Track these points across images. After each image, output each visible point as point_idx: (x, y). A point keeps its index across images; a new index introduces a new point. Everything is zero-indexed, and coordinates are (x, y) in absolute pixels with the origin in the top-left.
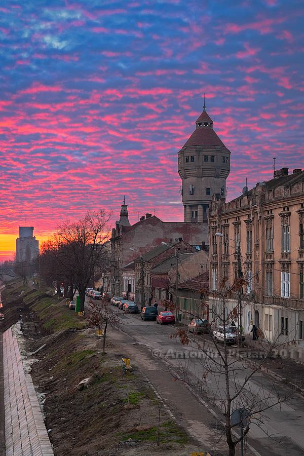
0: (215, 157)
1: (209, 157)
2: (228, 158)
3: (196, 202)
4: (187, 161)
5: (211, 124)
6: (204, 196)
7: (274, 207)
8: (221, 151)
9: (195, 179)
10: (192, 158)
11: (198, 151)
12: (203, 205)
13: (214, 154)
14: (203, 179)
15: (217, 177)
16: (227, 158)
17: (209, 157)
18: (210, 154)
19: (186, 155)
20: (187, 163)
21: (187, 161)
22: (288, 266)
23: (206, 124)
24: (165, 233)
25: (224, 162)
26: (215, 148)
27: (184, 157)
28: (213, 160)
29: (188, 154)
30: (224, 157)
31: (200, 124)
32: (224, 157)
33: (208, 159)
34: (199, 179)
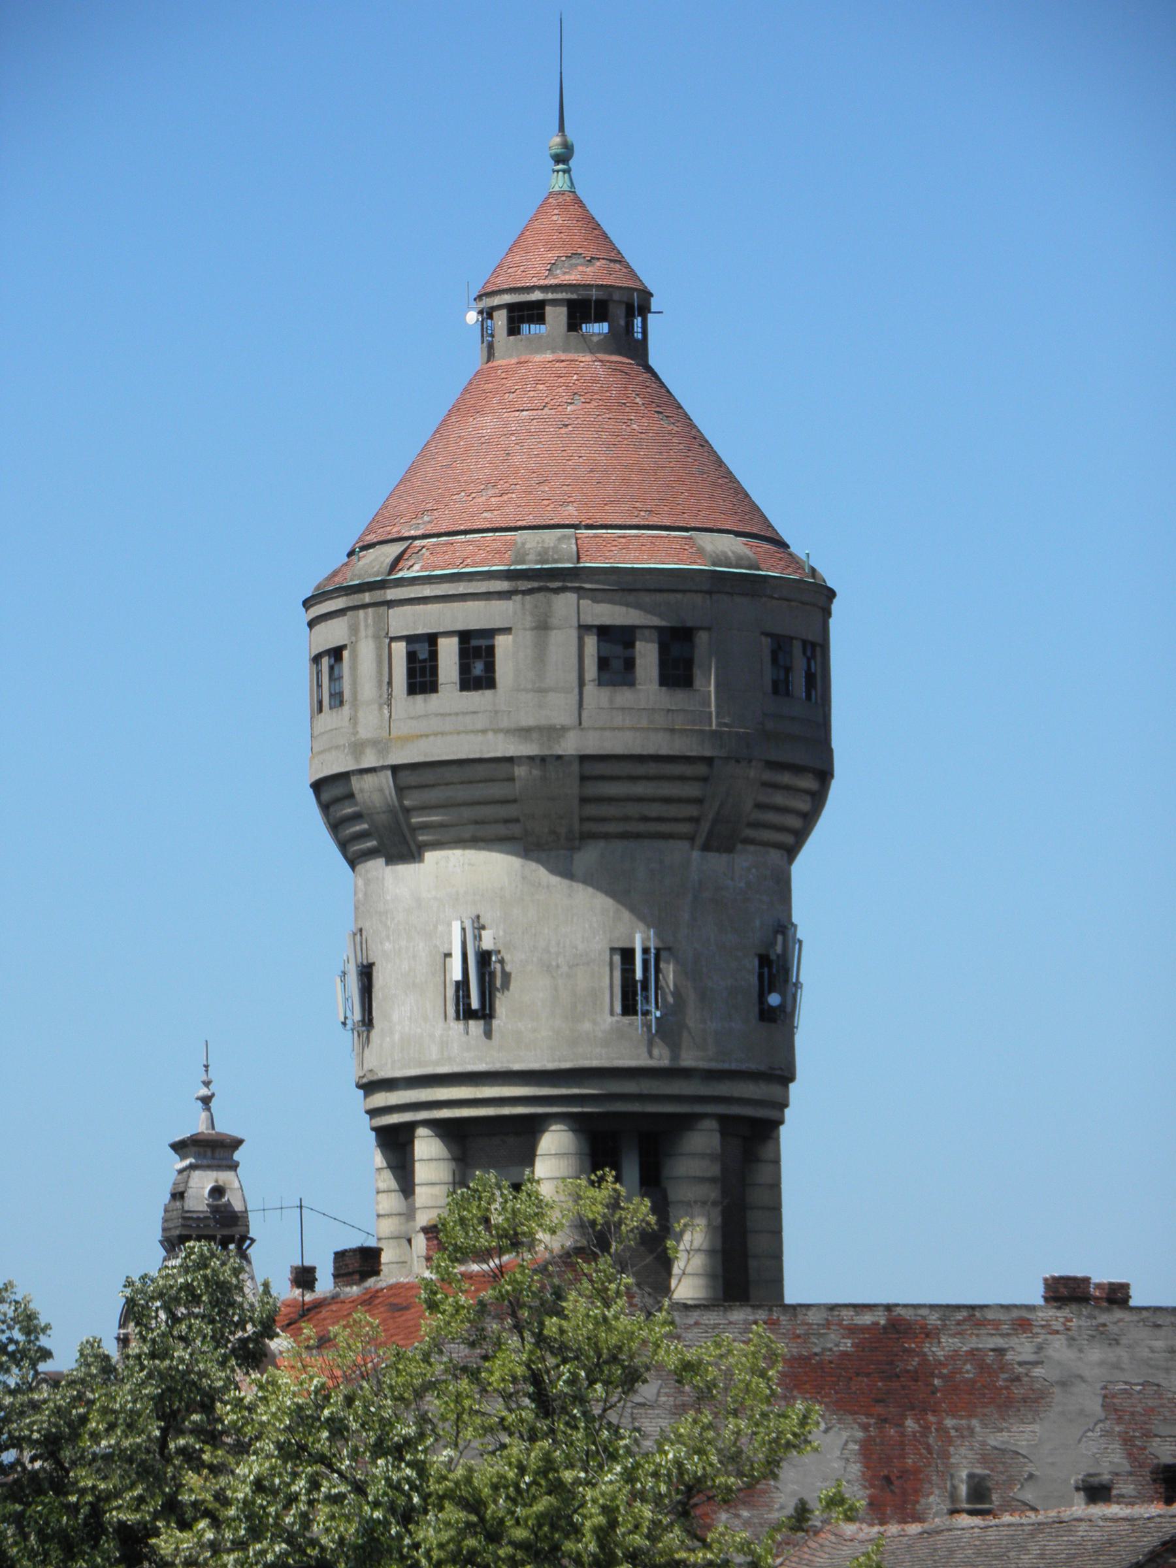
0: (702, 638)
4: (422, 678)
10: (477, 651)
25: (781, 688)
33: (630, 664)
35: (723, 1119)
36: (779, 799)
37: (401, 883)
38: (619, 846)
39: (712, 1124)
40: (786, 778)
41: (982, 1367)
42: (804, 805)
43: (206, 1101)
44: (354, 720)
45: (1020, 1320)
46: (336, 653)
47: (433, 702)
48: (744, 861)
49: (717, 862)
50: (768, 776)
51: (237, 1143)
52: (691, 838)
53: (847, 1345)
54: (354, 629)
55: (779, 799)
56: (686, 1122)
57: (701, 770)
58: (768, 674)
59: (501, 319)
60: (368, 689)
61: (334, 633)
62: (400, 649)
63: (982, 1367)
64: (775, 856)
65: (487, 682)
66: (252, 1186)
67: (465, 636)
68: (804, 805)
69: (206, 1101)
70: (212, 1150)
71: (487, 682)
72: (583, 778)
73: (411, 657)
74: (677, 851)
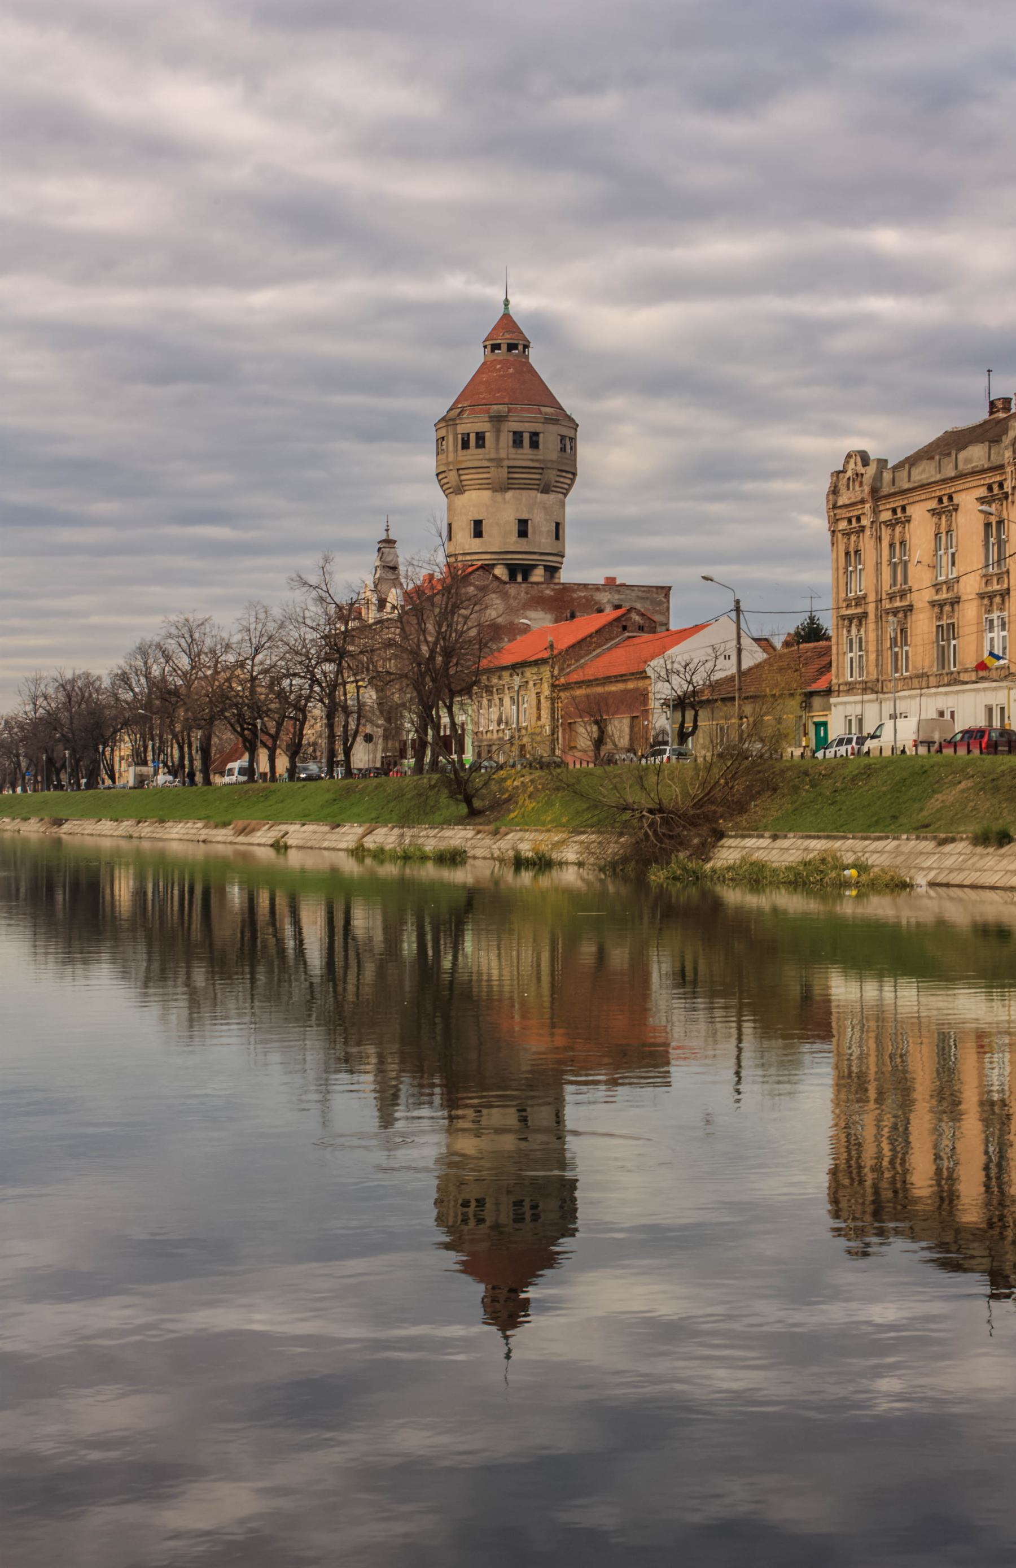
0: (541, 435)
1: (526, 437)
2: (573, 440)
3: (494, 557)
4: (465, 445)
5: (526, 347)
6: (513, 542)
7: (911, 500)
8: (555, 421)
9: (487, 494)
10: (480, 437)
11: (498, 420)
12: (508, 566)
13: (537, 427)
14: (509, 494)
15: (546, 490)
16: (571, 439)
17: (526, 437)
18: (527, 427)
19: (461, 429)
20: (465, 452)
21: (465, 445)
22: (1003, 601)
23: (511, 347)
24: (510, 610)
25: (563, 449)
26: (541, 413)
27: (456, 435)
28: (534, 445)
29: (471, 425)
30: (563, 438)
31: (496, 347)
32: (563, 438)
33: (521, 442)
34: (499, 496)
35: (545, 566)
36: (562, 480)
37: (461, 500)
38: (518, 491)
39: (542, 567)
40: (564, 474)
41: (587, 600)
42: (569, 482)
43: (387, 530)
44: (447, 457)
45: (597, 588)
46: (443, 438)
47: (469, 452)
48: (551, 498)
49: (545, 496)
50: (559, 473)
51: (395, 542)
52: (537, 490)
53: (552, 593)
54: (447, 432)
55: (562, 480)
56: (535, 566)
57: (540, 471)
58: (560, 446)
59: (489, 347)
60: (451, 448)
61: (443, 433)
62: (460, 436)
63: (587, 600)
64: (561, 496)
65: (483, 446)
66: (403, 555)
67: (477, 434)
68: (569, 482)
69: (387, 530)
70: (738, 1101)
71: (483, 446)
72: (509, 473)
73: (463, 439)
74: (533, 493)
